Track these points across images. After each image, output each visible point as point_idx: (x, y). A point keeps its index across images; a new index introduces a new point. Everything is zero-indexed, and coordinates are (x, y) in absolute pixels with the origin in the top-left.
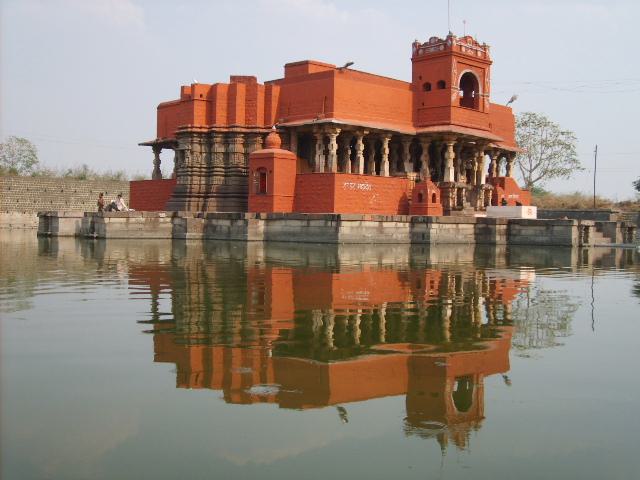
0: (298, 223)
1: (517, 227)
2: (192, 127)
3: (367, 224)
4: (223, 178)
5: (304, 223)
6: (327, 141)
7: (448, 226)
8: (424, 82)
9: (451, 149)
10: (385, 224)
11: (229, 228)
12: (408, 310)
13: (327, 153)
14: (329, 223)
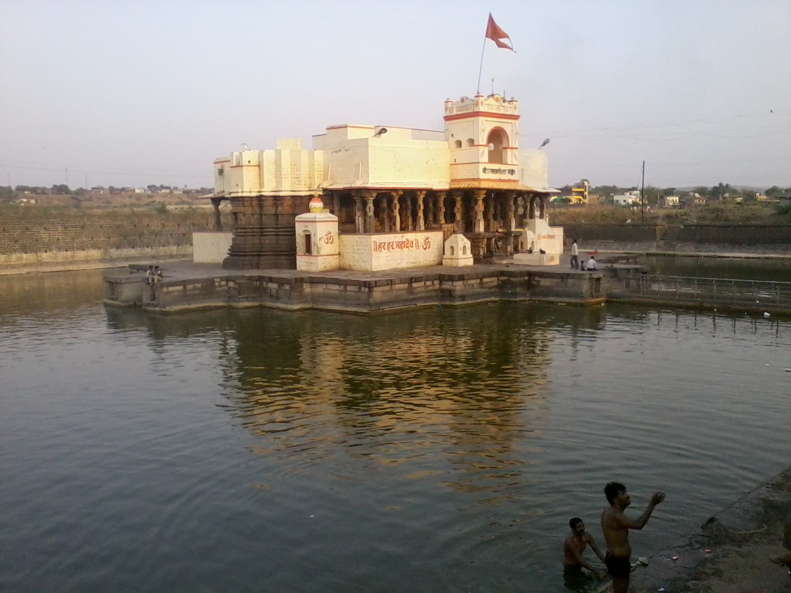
0: (336, 287)
1: (537, 278)
2: (242, 192)
3: (398, 286)
4: (274, 237)
5: (342, 287)
6: (365, 204)
7: (472, 282)
8: (455, 140)
9: (480, 203)
10: (414, 285)
11: (277, 291)
12: (326, 381)
13: (365, 214)
14: (363, 289)
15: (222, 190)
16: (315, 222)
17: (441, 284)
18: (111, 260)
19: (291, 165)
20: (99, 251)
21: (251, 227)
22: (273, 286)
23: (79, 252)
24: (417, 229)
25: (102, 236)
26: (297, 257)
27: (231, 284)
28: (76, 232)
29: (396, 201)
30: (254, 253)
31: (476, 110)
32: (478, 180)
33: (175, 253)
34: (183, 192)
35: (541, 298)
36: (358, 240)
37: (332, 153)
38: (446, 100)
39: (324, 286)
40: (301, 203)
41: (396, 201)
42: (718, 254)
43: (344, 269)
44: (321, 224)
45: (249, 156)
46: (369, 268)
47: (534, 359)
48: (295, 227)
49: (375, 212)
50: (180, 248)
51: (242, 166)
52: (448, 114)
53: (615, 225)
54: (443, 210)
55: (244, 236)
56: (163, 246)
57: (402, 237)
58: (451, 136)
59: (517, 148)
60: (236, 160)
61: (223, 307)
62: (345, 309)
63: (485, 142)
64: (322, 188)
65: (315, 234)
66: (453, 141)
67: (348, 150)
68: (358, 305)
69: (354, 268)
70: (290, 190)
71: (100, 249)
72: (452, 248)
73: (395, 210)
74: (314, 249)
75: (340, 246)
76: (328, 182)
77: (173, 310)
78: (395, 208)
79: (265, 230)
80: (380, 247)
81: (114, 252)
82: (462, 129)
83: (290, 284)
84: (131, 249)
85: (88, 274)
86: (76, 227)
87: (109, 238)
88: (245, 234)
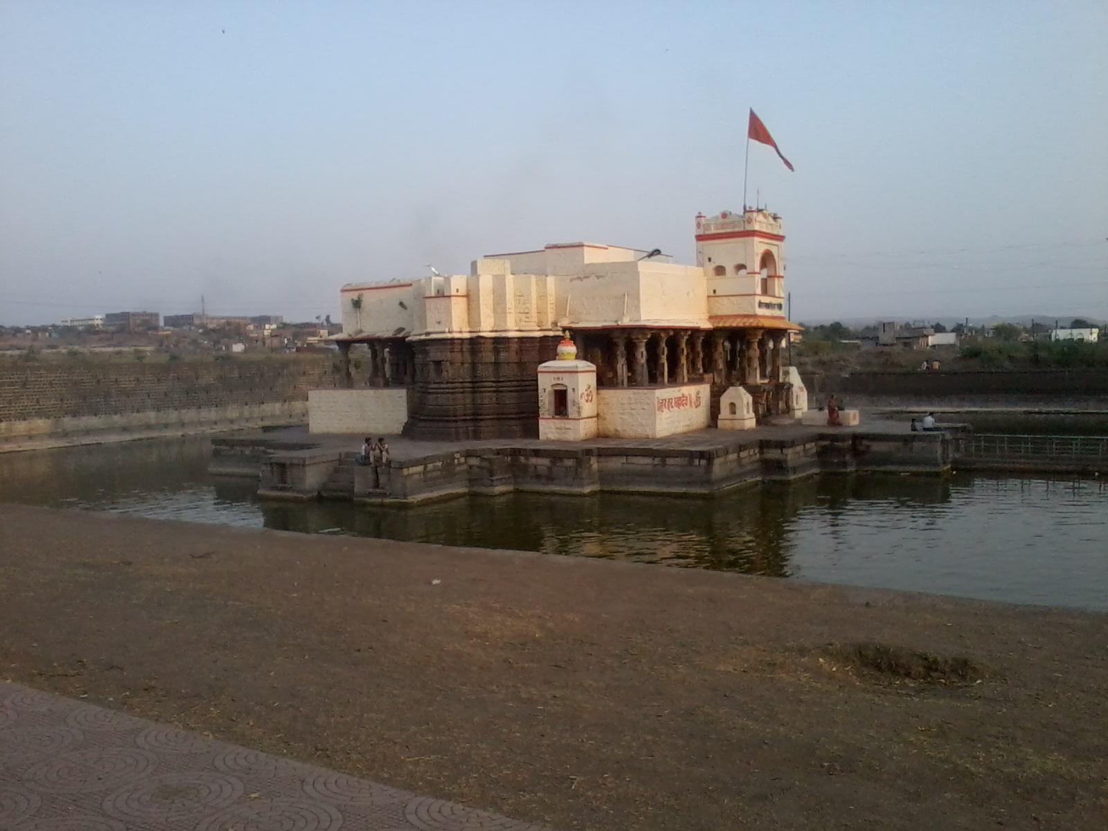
0: (648, 460)
1: (865, 442)
14: (696, 462)
15: (359, 327)
16: (577, 372)
17: (761, 453)
18: (65, 434)
19: (515, 296)
20: (47, 420)
21: (461, 380)
22: (544, 462)
23: (18, 422)
24: (679, 379)
25: (51, 398)
26: (540, 421)
27: (474, 461)
28: (14, 393)
29: (663, 345)
30: (468, 418)
31: (749, 228)
32: (755, 316)
33: (153, 422)
34: (1024, 328)
35: (875, 468)
36: (631, 396)
37: (571, 281)
38: (697, 214)
39: (624, 460)
40: (546, 347)
41: (663, 345)
42: (904, 408)
43: (606, 437)
44: (573, 371)
45: (458, 283)
46: (649, 433)
47: (616, 556)
48: (537, 380)
49: (648, 361)
50: (161, 414)
51: (449, 297)
52: (701, 232)
53: (861, 374)
54: (701, 355)
55: (452, 393)
56: (138, 412)
57: (679, 391)
58: (707, 260)
59: (782, 277)
60: (435, 288)
61: (463, 495)
62: (665, 490)
63: (757, 269)
64: (561, 327)
65: (574, 389)
66: (711, 267)
67: (601, 276)
68: (689, 484)
69: (622, 434)
70: (516, 329)
71: (48, 418)
72: (733, 405)
73: (662, 356)
74: (571, 410)
75: (598, 404)
76: (567, 319)
77: (415, 501)
78: (663, 354)
79: (478, 384)
80: (665, 404)
81: (68, 422)
82: (725, 252)
83: (576, 458)
84: (94, 417)
85: (33, 456)
86: (12, 384)
87: (62, 400)
88: (453, 391)
